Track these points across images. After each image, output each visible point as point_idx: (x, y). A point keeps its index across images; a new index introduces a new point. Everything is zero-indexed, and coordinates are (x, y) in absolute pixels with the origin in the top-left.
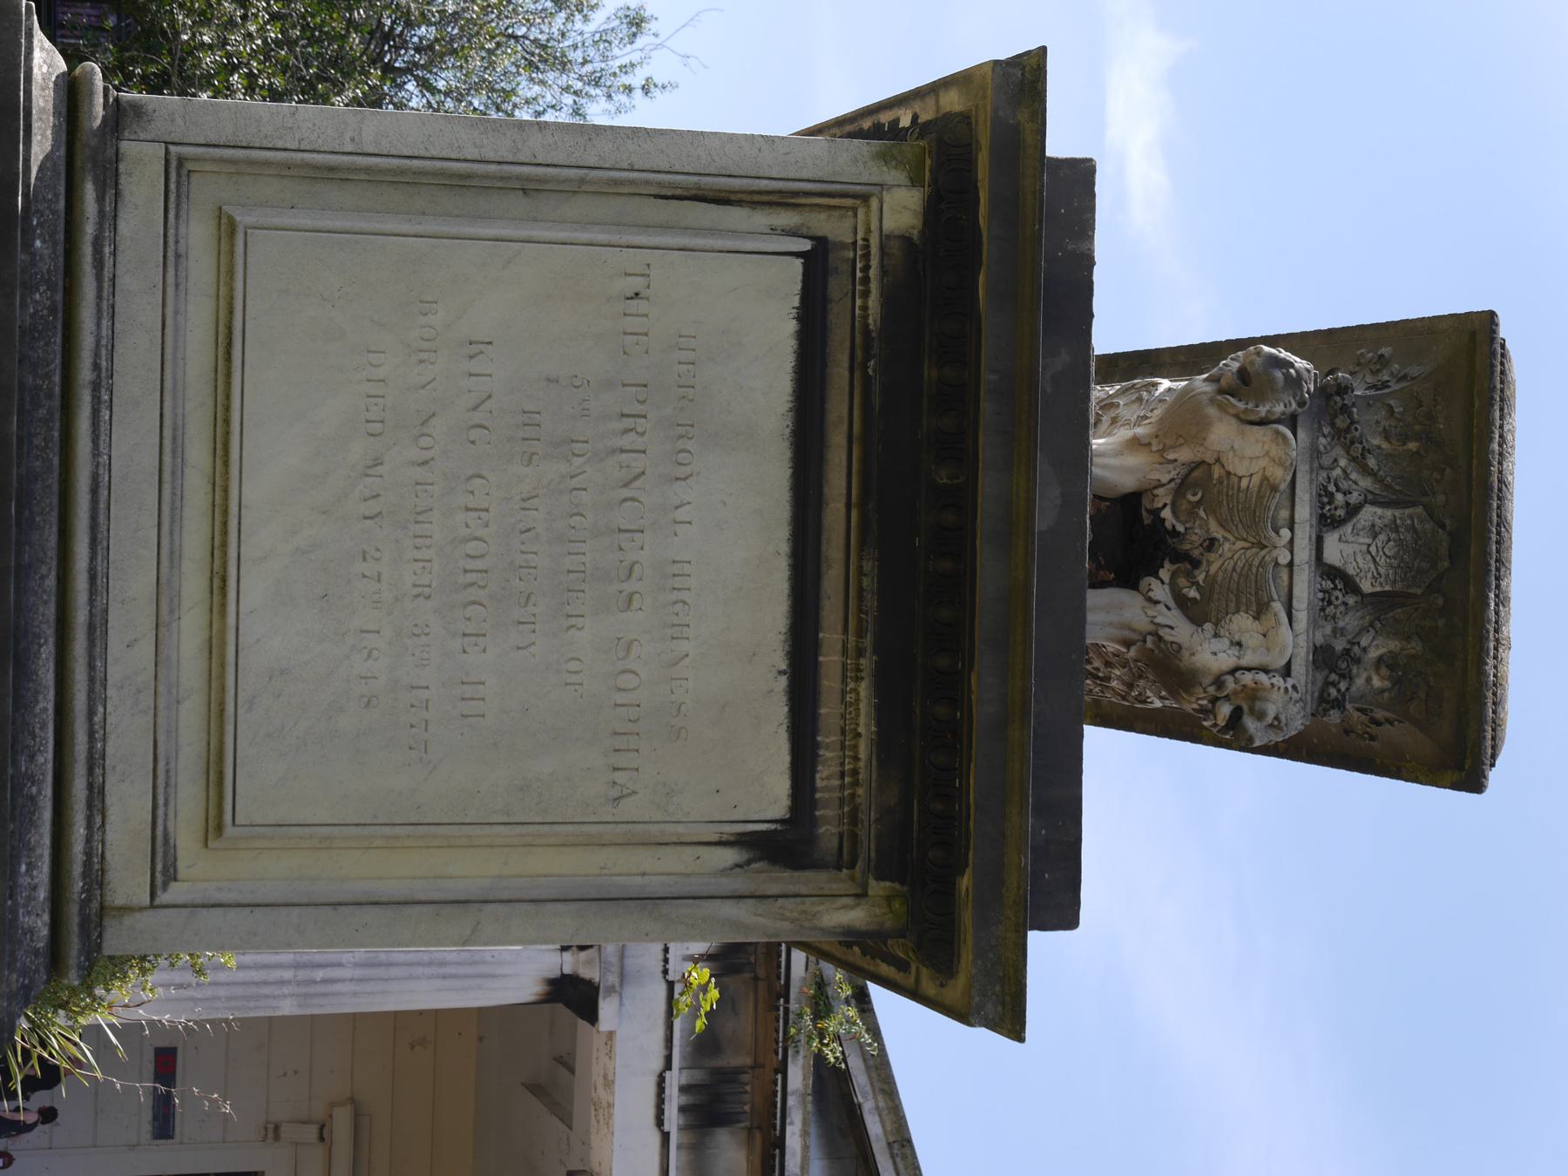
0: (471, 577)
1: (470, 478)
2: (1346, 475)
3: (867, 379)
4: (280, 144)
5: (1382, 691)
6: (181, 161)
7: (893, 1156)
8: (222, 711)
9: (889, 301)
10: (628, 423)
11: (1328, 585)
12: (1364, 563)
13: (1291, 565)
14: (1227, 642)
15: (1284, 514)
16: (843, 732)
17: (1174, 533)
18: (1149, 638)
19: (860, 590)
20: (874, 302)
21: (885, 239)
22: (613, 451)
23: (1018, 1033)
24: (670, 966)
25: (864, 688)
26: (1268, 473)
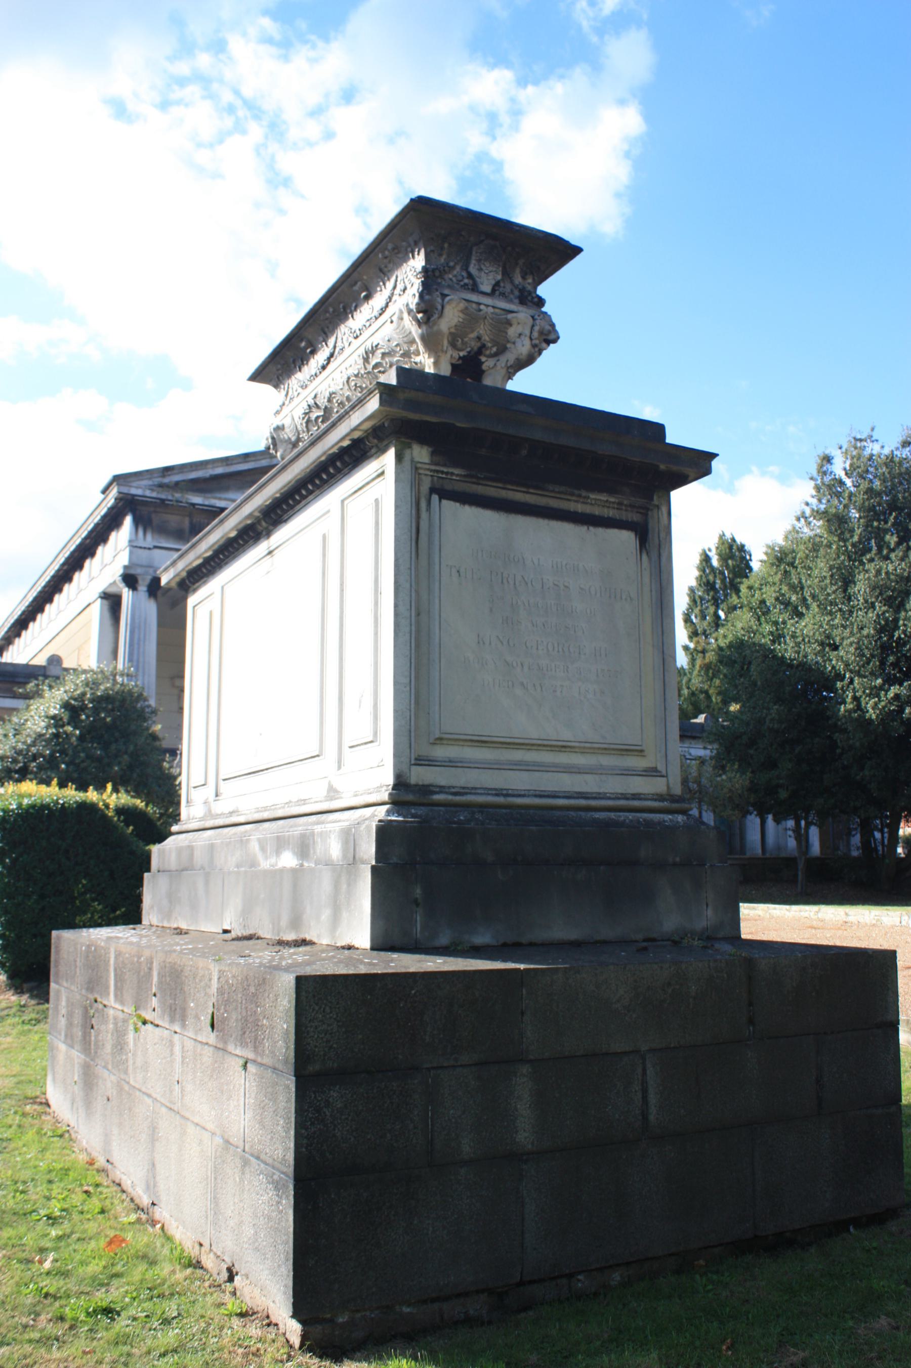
0: (560, 650)
1: (527, 647)
2: (455, 276)
3: (486, 478)
4: (408, 718)
5: (534, 279)
6: (416, 759)
7: (232, 464)
8: (605, 749)
9: (456, 465)
10: (505, 581)
11: (497, 293)
12: (491, 277)
13: (493, 307)
14: (518, 340)
15: (474, 306)
16: (603, 506)
17: (469, 352)
18: (510, 370)
19: (559, 492)
20: (456, 471)
21: (433, 463)
22: (515, 588)
23: (716, 455)
24: (147, 546)
25: (592, 496)
26: (460, 309)
